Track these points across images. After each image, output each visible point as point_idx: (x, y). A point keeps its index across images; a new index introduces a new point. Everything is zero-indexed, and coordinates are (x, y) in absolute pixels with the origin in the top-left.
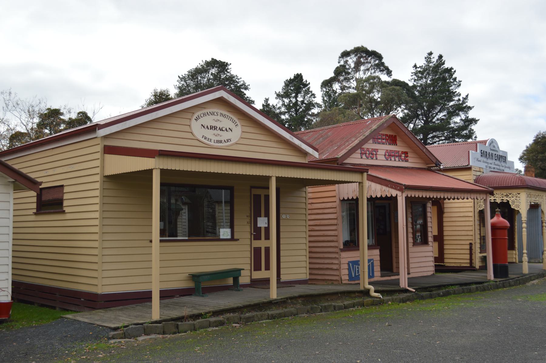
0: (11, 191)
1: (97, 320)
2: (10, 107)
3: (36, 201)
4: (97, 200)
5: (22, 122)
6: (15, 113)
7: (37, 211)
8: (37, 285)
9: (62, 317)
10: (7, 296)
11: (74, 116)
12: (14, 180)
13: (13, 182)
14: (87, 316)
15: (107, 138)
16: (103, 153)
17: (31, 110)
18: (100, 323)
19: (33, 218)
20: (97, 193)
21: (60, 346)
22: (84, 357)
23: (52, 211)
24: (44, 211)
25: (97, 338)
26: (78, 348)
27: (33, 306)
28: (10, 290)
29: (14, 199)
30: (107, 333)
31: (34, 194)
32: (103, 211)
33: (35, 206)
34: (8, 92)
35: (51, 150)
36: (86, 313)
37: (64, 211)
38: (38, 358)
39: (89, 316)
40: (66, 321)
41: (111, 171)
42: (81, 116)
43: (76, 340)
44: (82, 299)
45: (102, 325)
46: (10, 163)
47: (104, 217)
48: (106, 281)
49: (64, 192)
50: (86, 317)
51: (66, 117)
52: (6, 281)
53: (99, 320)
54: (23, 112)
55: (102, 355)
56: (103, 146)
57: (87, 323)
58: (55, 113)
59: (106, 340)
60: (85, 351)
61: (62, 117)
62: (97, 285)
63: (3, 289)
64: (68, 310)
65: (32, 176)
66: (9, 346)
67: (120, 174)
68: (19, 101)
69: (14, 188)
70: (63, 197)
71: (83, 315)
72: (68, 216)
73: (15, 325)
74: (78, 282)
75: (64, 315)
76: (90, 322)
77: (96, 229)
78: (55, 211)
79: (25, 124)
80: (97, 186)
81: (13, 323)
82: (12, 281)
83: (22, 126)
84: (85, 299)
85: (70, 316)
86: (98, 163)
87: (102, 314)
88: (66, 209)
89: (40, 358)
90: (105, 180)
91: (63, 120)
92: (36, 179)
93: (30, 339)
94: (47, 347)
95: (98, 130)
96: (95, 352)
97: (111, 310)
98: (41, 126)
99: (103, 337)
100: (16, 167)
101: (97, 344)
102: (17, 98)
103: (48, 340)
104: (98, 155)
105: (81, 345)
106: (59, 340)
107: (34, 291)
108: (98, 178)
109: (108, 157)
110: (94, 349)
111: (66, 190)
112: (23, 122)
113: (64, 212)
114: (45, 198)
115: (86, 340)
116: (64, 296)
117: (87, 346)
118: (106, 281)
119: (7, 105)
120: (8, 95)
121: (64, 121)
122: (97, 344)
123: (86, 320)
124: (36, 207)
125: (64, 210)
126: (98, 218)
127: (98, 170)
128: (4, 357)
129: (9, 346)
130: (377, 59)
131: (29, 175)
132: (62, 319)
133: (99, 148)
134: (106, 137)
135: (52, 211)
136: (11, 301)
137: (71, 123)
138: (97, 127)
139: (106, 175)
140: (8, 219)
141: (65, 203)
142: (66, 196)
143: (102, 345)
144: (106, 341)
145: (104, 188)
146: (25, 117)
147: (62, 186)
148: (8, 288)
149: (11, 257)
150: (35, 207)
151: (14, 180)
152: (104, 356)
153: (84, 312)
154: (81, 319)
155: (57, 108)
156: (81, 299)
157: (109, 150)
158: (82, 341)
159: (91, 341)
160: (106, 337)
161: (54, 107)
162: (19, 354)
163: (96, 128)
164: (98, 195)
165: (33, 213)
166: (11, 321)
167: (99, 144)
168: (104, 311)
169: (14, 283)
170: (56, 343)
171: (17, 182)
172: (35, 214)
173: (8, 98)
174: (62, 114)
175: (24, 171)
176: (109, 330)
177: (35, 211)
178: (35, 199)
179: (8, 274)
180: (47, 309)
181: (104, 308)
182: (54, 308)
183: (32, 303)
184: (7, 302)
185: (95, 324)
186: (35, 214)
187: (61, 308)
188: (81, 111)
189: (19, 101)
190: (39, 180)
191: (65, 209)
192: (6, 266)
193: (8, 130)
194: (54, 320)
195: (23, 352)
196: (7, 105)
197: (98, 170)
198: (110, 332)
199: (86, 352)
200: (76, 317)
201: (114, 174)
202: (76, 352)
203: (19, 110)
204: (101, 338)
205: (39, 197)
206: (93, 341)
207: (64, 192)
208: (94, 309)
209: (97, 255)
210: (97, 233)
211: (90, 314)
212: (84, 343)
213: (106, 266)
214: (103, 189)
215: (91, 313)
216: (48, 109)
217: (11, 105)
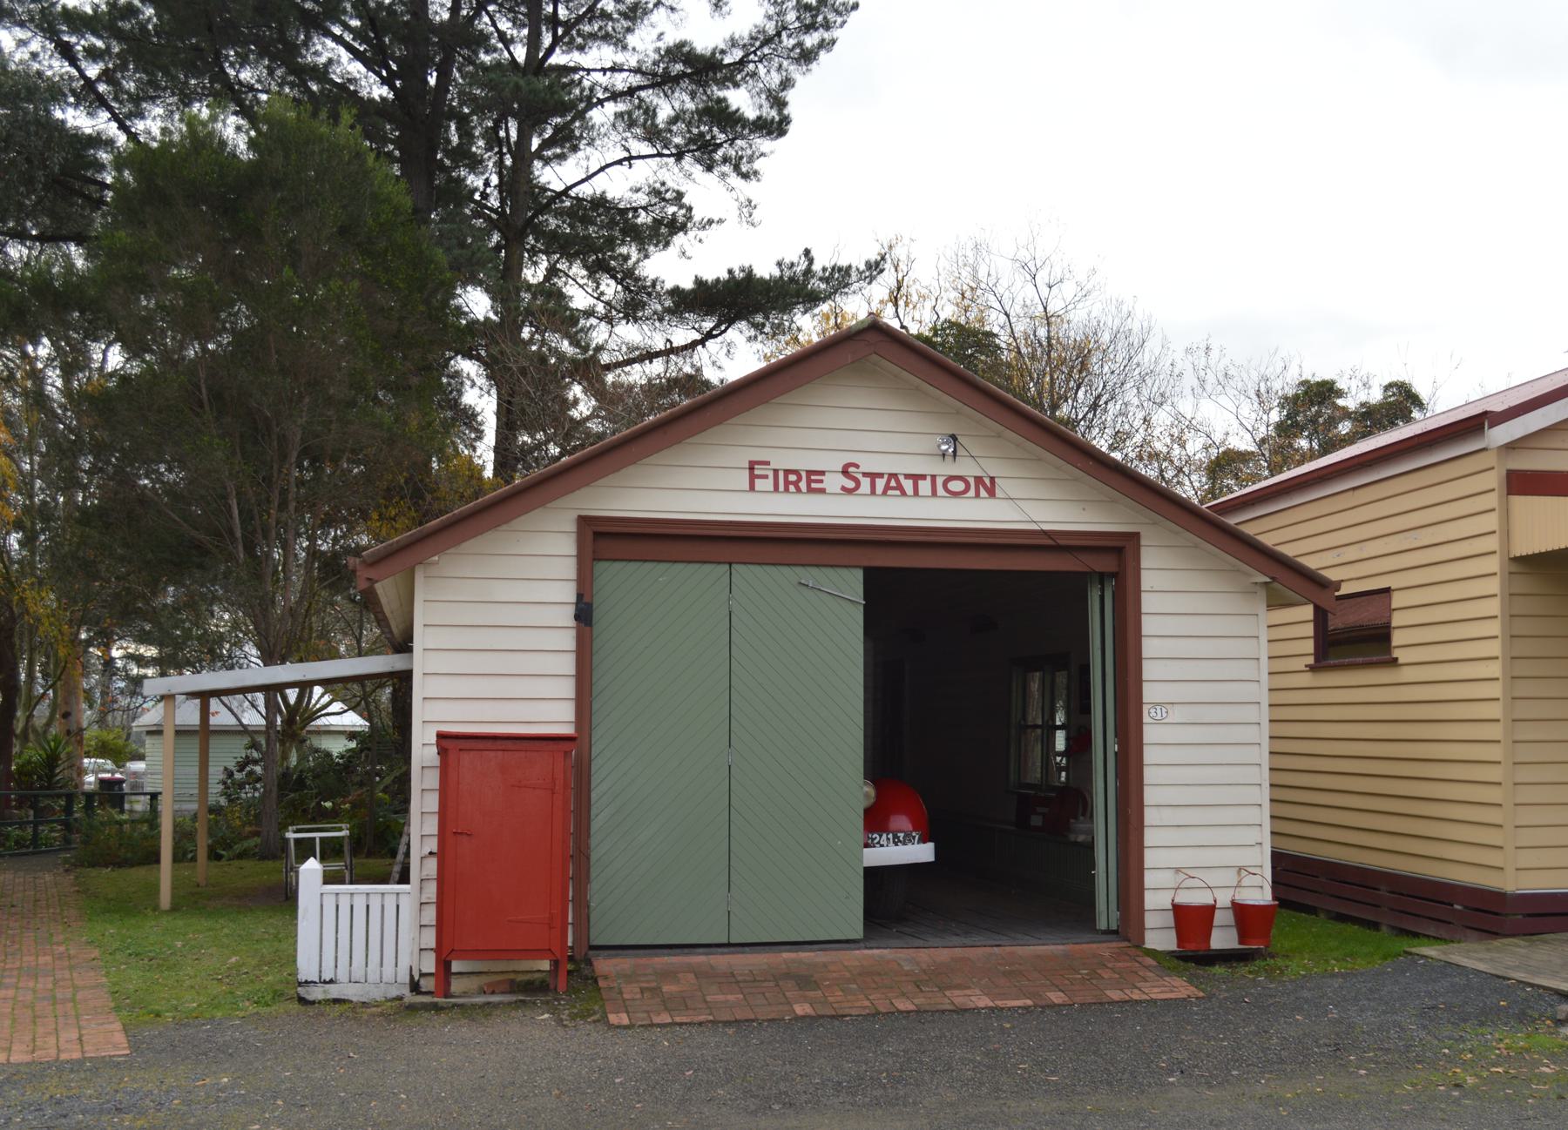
0: (1261, 607)
1: (1508, 968)
2: (1209, 387)
3: (1311, 633)
4: (1494, 628)
5: (1241, 424)
6: (1223, 400)
7: (1317, 660)
8: (1386, 873)
9: (1410, 954)
10: (1261, 887)
11: (1376, 396)
12: (1268, 580)
13: (1266, 583)
14: (1481, 956)
15: (1514, 448)
16: (1505, 492)
17: (1263, 390)
18: (1523, 975)
19: (1307, 679)
20: (1493, 607)
21: (1423, 1034)
22: (1500, 1070)
23: (1360, 660)
24: (1336, 661)
25: (1523, 1018)
26: (1476, 1043)
27: (1314, 916)
28: (1268, 872)
29: (1269, 627)
30: (1551, 1006)
31: (1307, 612)
32: (1512, 658)
33: (1309, 646)
34: (1203, 347)
35: (1351, 493)
36: (1476, 946)
37: (1396, 659)
38: (1371, 1060)
39: (1487, 956)
40: (1424, 965)
41: (1531, 542)
42: (1394, 395)
43: (1465, 1021)
44: (1457, 907)
45: (1531, 981)
46: (1249, 530)
47: (1515, 674)
48: (1527, 859)
49: (1393, 606)
50: (1476, 955)
51: (1350, 403)
52: (1257, 848)
53: (1518, 967)
54: (1242, 397)
55: (1548, 1067)
56: (1505, 472)
57: (1486, 973)
58: (1321, 393)
59: (1549, 1027)
60: (1497, 1052)
61: (1340, 402)
62: (1502, 869)
63: (1250, 870)
64: (1416, 935)
65: (1311, 563)
66: (1285, 1022)
67: (1560, 550)
68: (1231, 367)
69: (1267, 601)
70: (1389, 623)
71: (1469, 951)
72: (1407, 674)
73: (1287, 967)
74: (1444, 857)
75: (1414, 946)
76: (1493, 972)
77: (1494, 710)
78: (1367, 659)
79: (1251, 429)
80: (1493, 586)
81: (1280, 962)
82: (1272, 852)
83: (1243, 432)
84: (1465, 907)
85: (1431, 951)
86: (1491, 522)
87: (1523, 951)
88: (1401, 655)
89: (1377, 1063)
90: (1513, 570)
91: (1344, 409)
92: (1320, 572)
93: (1336, 1006)
94: (1388, 1032)
95: (1490, 427)
96: (1527, 1058)
97: (1546, 942)
98: (1287, 429)
99: (1541, 1016)
100: (1268, 540)
101: (1528, 1036)
102: (1225, 362)
103: (1384, 1012)
104: (1492, 500)
105: (1483, 1035)
106: (1416, 1016)
107: (1317, 877)
108: (1493, 564)
109: (1520, 502)
110: (1521, 1048)
111: (1397, 600)
112: (1246, 424)
113: (1394, 662)
114: (1335, 623)
115: (1492, 1021)
116: (1403, 895)
117: (1501, 1040)
118: (1527, 859)
119: (1202, 382)
120: (1203, 354)
121: (1346, 414)
122: (1528, 1036)
123: (1482, 967)
124: (1312, 651)
125: (1395, 656)
126: (1497, 679)
127: (1492, 543)
128: (1279, 1051)
129: (1285, 1022)
130: (109, 345)
131: (1301, 560)
132: (1410, 957)
133: (1493, 480)
134: (1512, 447)
135: (1360, 660)
136: (1272, 903)
137: (1372, 418)
138: (1472, 426)
139: (1518, 555)
140: (1256, 684)
141: (1398, 638)
142: (1397, 619)
143: (1542, 1039)
144: (1552, 1030)
145: (1512, 592)
146: (1248, 411)
147: (1387, 591)
148: (1261, 866)
149: (1266, 785)
150: (1312, 650)
151: (1268, 580)
152: (1557, 1073)
153: (1465, 941)
154: (1466, 960)
155: (1327, 377)
156: (1452, 905)
157: (1522, 483)
158: (1482, 1024)
159: (1506, 1024)
160: (1548, 1018)
161: (1322, 374)
162: (1319, 1047)
163: (1484, 424)
164: (1495, 614)
165: (1306, 666)
166: (1272, 956)
167: (1493, 468)
168: (1527, 944)
169: (1278, 858)
170: (1411, 1024)
171: (1276, 585)
172: (1312, 669)
173: (1203, 362)
174: (1340, 393)
175: (1289, 551)
176: (1555, 997)
177: (1311, 660)
178: (1309, 630)
179: (1261, 831)
180: (1356, 927)
181: (1525, 935)
182: (1375, 926)
183: (1311, 910)
184: (1262, 903)
185: (1509, 979)
186: (1312, 669)
187: (1393, 928)
188: (1394, 379)
189: (1231, 367)
190: (1333, 575)
191: (1396, 653)
192: (1256, 809)
193: (1206, 448)
194: (1386, 959)
195: (1327, 1041)
196: (1202, 382)
197: (1492, 543)
198: (1560, 1003)
199: (1499, 1056)
200: (1451, 956)
201: (1543, 550)
202: (1471, 1052)
203: (1231, 392)
204: (1534, 1021)
205: (1321, 617)
206: (1513, 1027)
207: (1393, 606)
208: (1495, 935)
209: (1500, 784)
210: (1498, 720)
211: (1488, 950)
212: (1490, 1030)
213: (1527, 817)
214: (1511, 596)
215: (1489, 946)
216: (1303, 383)
217: (1211, 379)
